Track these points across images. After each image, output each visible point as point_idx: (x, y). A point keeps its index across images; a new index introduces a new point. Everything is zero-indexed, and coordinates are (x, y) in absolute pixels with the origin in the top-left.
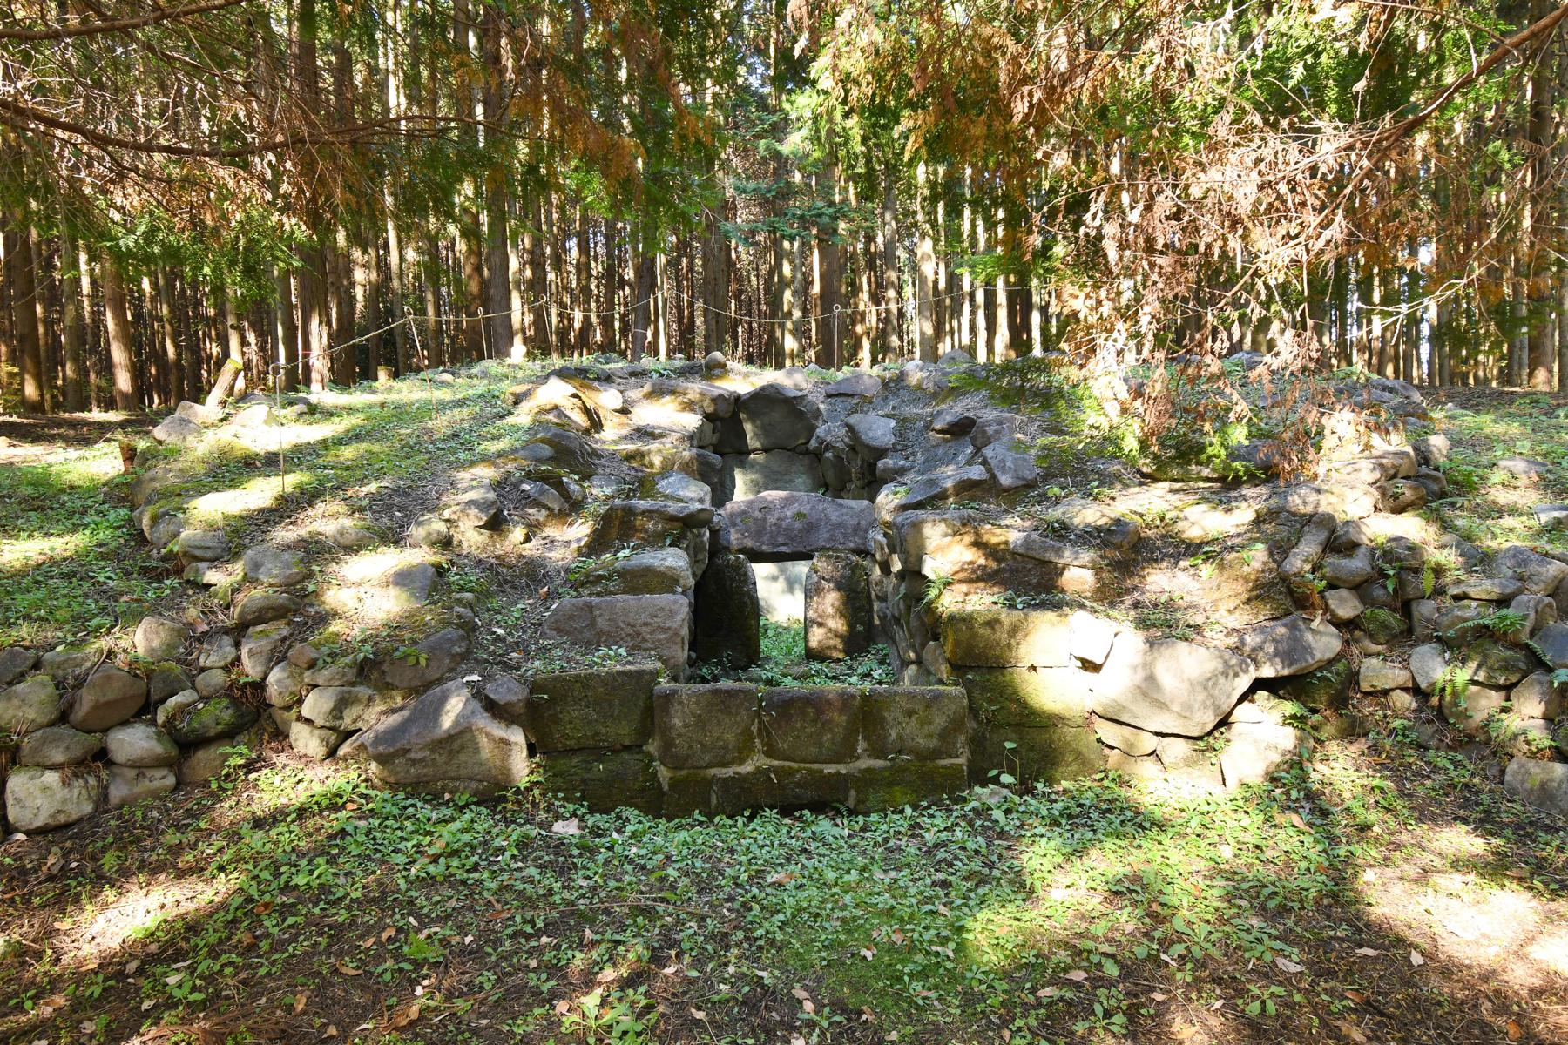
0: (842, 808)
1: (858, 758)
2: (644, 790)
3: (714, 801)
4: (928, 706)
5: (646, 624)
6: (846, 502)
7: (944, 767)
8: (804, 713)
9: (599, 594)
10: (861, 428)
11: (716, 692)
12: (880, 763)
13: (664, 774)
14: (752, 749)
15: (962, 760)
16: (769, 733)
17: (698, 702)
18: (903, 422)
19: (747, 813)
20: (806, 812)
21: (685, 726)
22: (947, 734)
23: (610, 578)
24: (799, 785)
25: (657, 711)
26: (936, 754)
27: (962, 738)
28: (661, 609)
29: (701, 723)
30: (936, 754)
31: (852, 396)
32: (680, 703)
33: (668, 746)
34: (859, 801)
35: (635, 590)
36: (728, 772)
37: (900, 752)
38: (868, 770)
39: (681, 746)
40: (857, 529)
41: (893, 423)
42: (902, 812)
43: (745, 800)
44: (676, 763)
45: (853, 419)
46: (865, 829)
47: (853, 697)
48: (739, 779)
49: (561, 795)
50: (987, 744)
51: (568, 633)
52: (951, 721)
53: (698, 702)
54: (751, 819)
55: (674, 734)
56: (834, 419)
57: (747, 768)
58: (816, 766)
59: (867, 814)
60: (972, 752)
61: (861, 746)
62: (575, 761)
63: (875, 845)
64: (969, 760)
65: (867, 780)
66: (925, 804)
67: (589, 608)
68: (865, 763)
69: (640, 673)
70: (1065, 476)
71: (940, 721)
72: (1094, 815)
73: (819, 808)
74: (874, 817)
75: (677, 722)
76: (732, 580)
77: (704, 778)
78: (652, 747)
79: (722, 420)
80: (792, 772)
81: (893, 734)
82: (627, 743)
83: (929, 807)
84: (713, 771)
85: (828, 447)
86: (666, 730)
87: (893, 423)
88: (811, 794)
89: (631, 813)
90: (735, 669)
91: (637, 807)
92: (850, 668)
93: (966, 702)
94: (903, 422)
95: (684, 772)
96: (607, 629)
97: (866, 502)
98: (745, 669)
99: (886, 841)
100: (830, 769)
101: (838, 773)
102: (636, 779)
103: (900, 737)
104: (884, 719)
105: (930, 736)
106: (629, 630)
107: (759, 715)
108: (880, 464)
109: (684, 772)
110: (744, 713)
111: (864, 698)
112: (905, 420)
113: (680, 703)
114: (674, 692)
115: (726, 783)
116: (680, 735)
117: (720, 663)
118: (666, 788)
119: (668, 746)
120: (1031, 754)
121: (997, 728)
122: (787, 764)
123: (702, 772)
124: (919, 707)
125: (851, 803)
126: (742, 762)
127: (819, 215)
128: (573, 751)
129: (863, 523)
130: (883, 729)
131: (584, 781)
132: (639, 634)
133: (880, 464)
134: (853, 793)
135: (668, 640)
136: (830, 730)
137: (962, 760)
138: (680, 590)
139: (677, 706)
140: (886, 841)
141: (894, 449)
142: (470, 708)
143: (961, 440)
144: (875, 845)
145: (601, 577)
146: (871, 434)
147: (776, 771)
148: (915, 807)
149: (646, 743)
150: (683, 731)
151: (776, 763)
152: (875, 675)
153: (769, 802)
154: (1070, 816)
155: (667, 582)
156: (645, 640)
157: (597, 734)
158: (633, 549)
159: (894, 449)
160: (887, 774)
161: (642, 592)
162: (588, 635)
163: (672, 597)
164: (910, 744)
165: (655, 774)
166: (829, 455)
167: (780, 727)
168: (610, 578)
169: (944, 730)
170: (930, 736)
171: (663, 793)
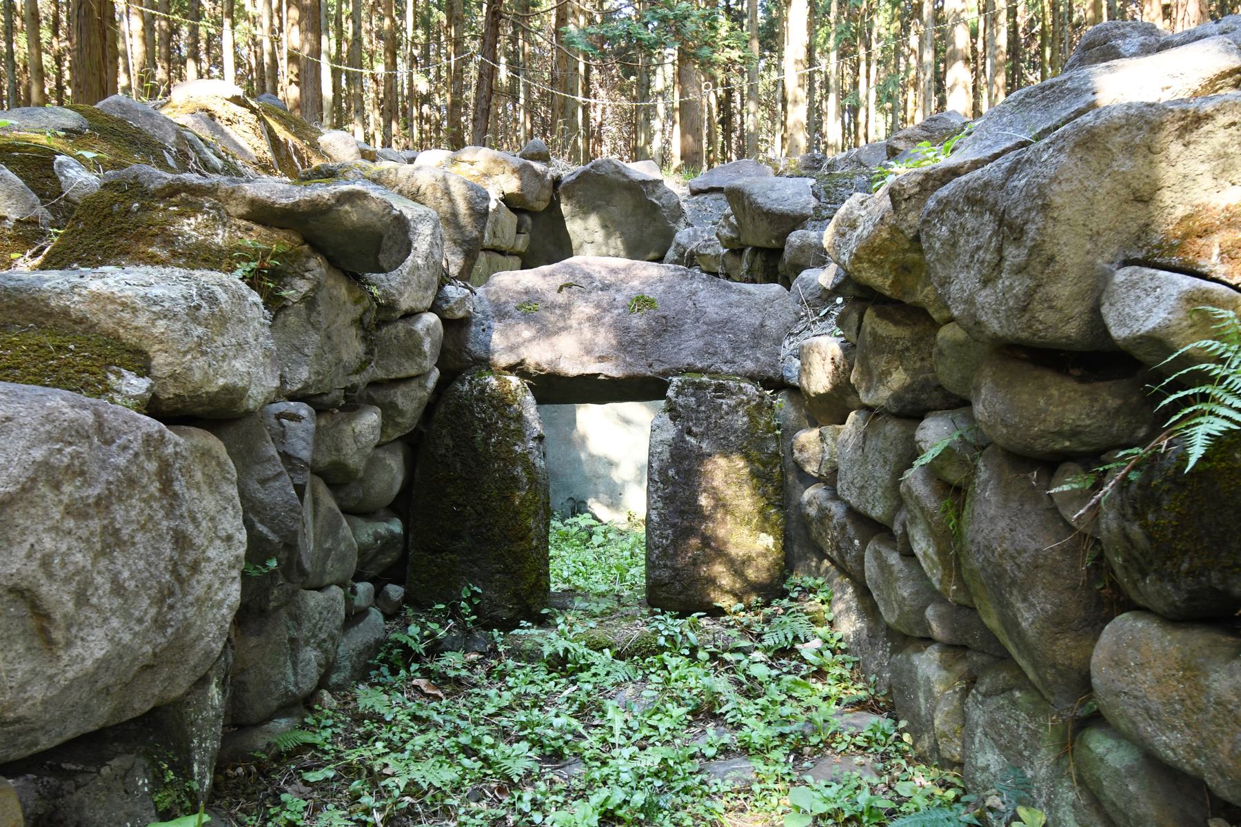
40: (758, 335)
76: (489, 428)
79: (533, 214)
98: (508, 626)
108: (795, 238)
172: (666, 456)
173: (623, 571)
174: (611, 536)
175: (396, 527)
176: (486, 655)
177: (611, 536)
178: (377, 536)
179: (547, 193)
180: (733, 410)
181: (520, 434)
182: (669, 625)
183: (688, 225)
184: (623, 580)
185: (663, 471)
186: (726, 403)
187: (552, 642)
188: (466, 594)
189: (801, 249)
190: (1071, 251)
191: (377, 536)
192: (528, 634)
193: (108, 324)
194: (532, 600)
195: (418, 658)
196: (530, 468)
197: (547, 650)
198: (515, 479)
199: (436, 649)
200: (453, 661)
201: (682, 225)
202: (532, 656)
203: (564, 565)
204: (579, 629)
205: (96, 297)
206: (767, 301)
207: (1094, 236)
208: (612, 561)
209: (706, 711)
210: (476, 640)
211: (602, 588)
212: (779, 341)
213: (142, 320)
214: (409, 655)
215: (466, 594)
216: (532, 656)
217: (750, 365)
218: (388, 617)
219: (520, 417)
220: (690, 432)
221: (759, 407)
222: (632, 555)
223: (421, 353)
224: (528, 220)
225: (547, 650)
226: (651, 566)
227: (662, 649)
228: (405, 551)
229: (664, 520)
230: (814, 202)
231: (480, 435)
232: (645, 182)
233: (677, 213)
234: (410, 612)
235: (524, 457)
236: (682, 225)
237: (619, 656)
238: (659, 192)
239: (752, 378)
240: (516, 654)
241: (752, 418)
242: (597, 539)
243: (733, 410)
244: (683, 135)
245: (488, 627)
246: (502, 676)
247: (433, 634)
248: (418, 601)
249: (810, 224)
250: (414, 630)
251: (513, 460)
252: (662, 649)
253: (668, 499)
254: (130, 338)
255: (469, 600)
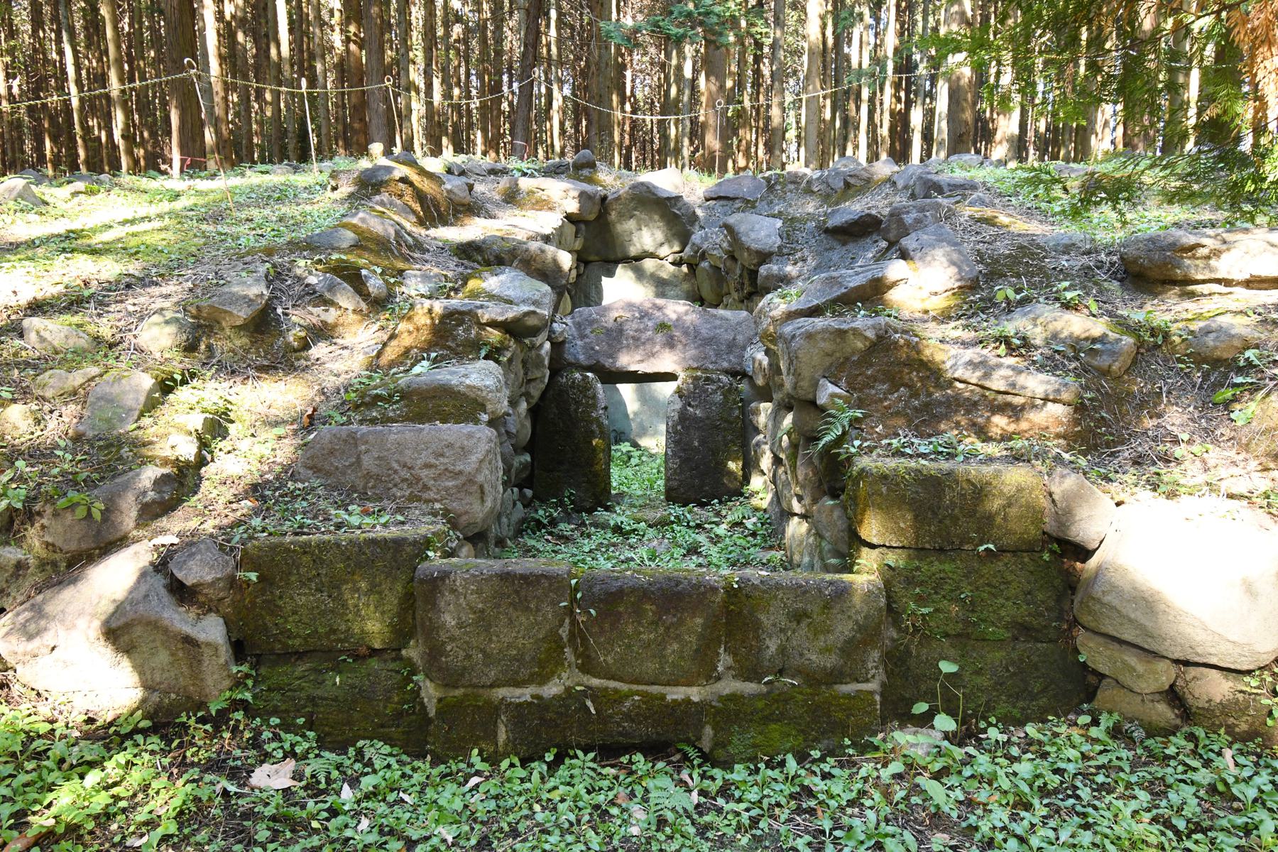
0: (692, 753)
1: (719, 679)
2: (399, 714)
3: (502, 736)
4: (827, 607)
5: (428, 466)
6: (721, 312)
7: (848, 696)
8: (638, 613)
9: (373, 421)
10: (742, 229)
11: (506, 577)
12: (750, 688)
13: (430, 692)
14: (560, 662)
15: (873, 686)
16: (584, 640)
17: (479, 592)
18: (791, 222)
19: (549, 757)
20: (639, 757)
21: (460, 625)
22: (852, 649)
23: (388, 399)
24: (627, 716)
25: (419, 603)
26: (836, 676)
27: (876, 654)
28: (450, 446)
29: (483, 622)
30: (836, 676)
31: (734, 199)
32: (453, 591)
33: (434, 653)
34: (718, 744)
35: (421, 417)
36: (525, 694)
37: (781, 672)
38: (733, 697)
39: (454, 654)
40: (732, 345)
41: (779, 223)
42: (782, 764)
43: (547, 736)
44: (449, 679)
45: (731, 220)
46: (725, 791)
47: (714, 590)
48: (540, 705)
49: (275, 721)
50: (912, 663)
51: (328, 474)
52: (860, 628)
53: (479, 592)
54: (553, 767)
55: (443, 636)
56: (712, 225)
57: (552, 689)
58: (655, 689)
59: (727, 766)
60: (889, 674)
61: (724, 660)
62: (301, 669)
63: (739, 828)
64: (883, 685)
65: (730, 713)
66: (816, 754)
67: (353, 440)
68: (730, 686)
69: (398, 543)
70: (1018, 276)
71: (843, 629)
72: (1085, 793)
73: (655, 750)
74: (739, 773)
75: (449, 620)
76: (578, 403)
77: (489, 702)
78: (413, 652)
79: (586, 223)
80: (620, 698)
81: (772, 645)
82: (377, 646)
83: (822, 760)
84: (502, 692)
85: (703, 256)
86: (431, 632)
87: (779, 223)
88: (647, 731)
89: (377, 751)
90: (578, 510)
91: (388, 740)
92: (718, 514)
93: (883, 601)
94: (791, 222)
95: (459, 692)
96: (375, 470)
97: (744, 313)
98: (590, 511)
99: (755, 822)
100: (676, 694)
101: (688, 701)
102: (388, 699)
103: (782, 650)
104: (757, 625)
105: (826, 650)
106: (405, 474)
107: (571, 612)
108: (763, 270)
109: (459, 692)
110: (548, 610)
111: (729, 590)
112: (793, 220)
113: (453, 591)
114: (444, 575)
115: (519, 712)
116: (452, 639)
117: (561, 503)
118: (432, 714)
119: (434, 653)
120: (979, 680)
121: (927, 639)
122: (613, 684)
123: (485, 693)
124: (814, 608)
125: (706, 745)
126: (543, 680)
127: (707, 14)
128: (300, 655)
129: (740, 338)
130: (757, 638)
131: (312, 700)
132: (418, 479)
133: (763, 270)
134: (708, 731)
135: (459, 489)
136: (678, 638)
137: (873, 686)
138: (485, 417)
139: (448, 597)
140: (755, 822)
141: (780, 253)
142: (143, 588)
143: (861, 243)
144: (739, 828)
145: (379, 397)
146: (753, 235)
147: (592, 693)
148: (802, 758)
149: (405, 645)
150: (457, 633)
151: (595, 682)
152: (749, 524)
153: (583, 741)
154: (1044, 792)
155: (464, 406)
156: (426, 488)
157: (334, 631)
158: (435, 361)
159: (780, 253)
160: (760, 705)
161: (430, 420)
162: (351, 477)
163: (468, 428)
164: (796, 662)
165: (416, 692)
166: (705, 264)
167: (602, 631)
168: (388, 399)
169: (849, 641)
170: (826, 650)
171: (430, 721)
172: (676, 418)
173: (652, 482)
174: (644, 458)
175: (528, 458)
176: (580, 525)
177: (644, 458)
178: (521, 463)
179: (596, 209)
180: (715, 392)
181: (594, 406)
182: (677, 510)
183: (702, 228)
184: (652, 488)
185: (674, 426)
186: (711, 388)
187: (613, 519)
188: (567, 494)
189: (767, 277)
190: (806, 373)
191: (521, 463)
192: (601, 514)
193: (473, 396)
194: (598, 495)
195: (544, 526)
196: (600, 425)
197: (612, 523)
198: (592, 432)
199: (554, 522)
200: (565, 528)
201: (697, 227)
202: (604, 526)
203: (617, 475)
204: (628, 513)
205: (468, 386)
206: (739, 324)
207: (814, 367)
208: (645, 476)
209: (693, 550)
210: (144, 718)
211: (639, 493)
212: (744, 348)
213: (484, 394)
214: (539, 525)
215: (567, 494)
216: (604, 526)
217: (725, 365)
218: (525, 506)
219: (594, 397)
220: (690, 405)
221: (729, 390)
222: (659, 472)
223: (544, 366)
224: (583, 227)
225: (612, 523)
226: (668, 480)
227: (673, 522)
228: (532, 470)
229: (675, 454)
230: (779, 242)
231: (573, 407)
232: (668, 199)
233: (694, 218)
234: (537, 503)
235: (597, 419)
236: (697, 227)
237: (650, 526)
238: (679, 205)
239: (726, 372)
240: (596, 525)
241: (725, 397)
242: (634, 461)
243: (715, 392)
244: (707, 79)
245: (579, 512)
246: (589, 536)
247: (551, 515)
248: (541, 498)
249: (775, 258)
250: (541, 512)
251: (590, 421)
252: (673, 522)
253: (677, 443)
254: (480, 400)
255: (569, 498)
